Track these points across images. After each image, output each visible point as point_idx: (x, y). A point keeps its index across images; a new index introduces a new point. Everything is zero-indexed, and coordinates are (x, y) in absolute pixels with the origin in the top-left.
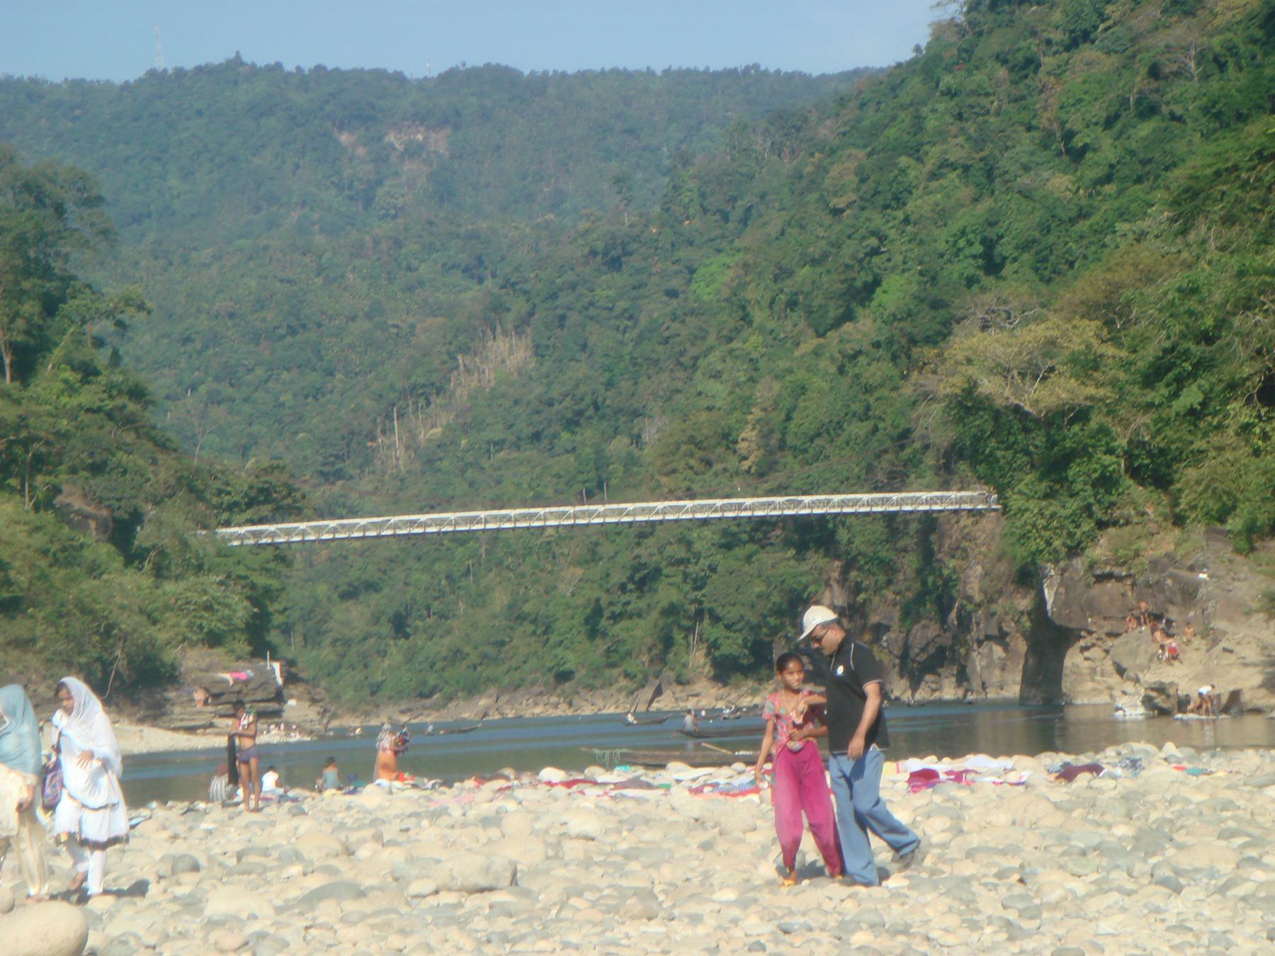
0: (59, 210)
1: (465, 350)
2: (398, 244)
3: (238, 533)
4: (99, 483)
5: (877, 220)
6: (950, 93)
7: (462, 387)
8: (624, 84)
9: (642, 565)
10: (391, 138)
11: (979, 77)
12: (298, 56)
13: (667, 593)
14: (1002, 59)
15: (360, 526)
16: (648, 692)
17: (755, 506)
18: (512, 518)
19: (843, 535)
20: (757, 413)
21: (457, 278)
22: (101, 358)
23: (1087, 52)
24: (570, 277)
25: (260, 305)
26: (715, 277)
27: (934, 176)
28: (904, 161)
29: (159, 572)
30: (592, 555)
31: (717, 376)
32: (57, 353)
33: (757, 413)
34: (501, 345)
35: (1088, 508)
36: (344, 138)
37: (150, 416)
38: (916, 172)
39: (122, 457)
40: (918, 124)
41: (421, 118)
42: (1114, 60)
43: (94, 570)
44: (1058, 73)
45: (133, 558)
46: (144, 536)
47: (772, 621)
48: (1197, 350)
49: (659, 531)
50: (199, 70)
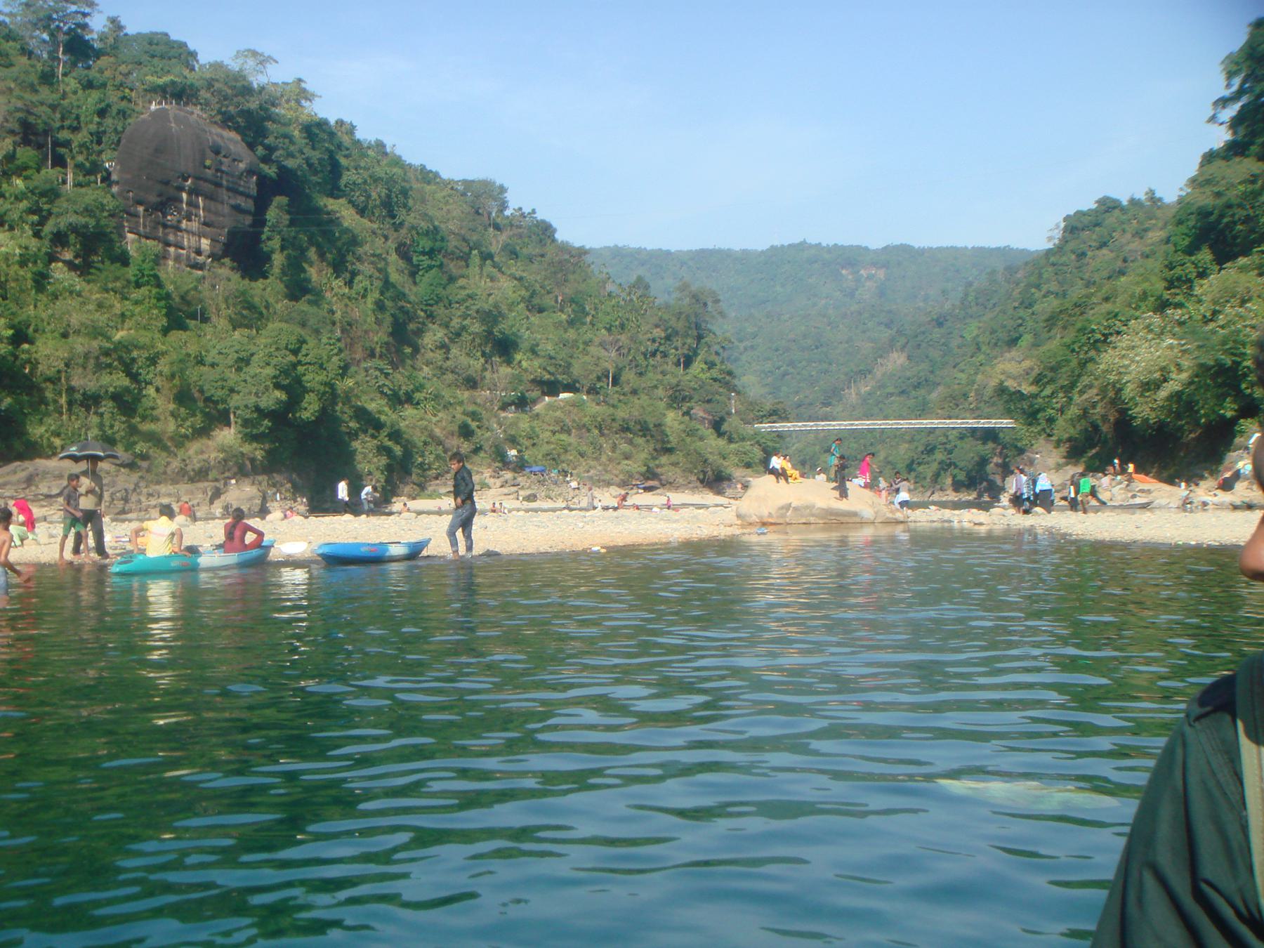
0: (705, 304)
1: (881, 357)
2: (860, 313)
3: (765, 427)
4: (708, 406)
5: (1021, 313)
6: (1053, 265)
7: (879, 372)
8: (955, 253)
9: (929, 445)
10: (862, 272)
11: (1064, 259)
12: (827, 240)
13: (939, 456)
14: (1073, 252)
15: (834, 425)
16: (929, 493)
17: (972, 423)
18: (891, 424)
19: (1001, 435)
20: (976, 386)
21: (882, 328)
22: (717, 360)
23: (1105, 251)
24: (922, 329)
25: (805, 336)
26: (972, 330)
27: (1044, 296)
28: (1033, 290)
29: (731, 440)
30: (912, 441)
31: (962, 371)
32: (699, 358)
33: (976, 386)
34: (895, 355)
35: (1044, 430)
36: (844, 272)
37: (736, 382)
38: (1038, 295)
39: (718, 397)
40: (1040, 275)
41: (874, 264)
42: (1112, 255)
43: (701, 439)
44: (1093, 258)
45: (720, 434)
46: (725, 427)
47: (57, 442)
48: (1050, 375)
49: (937, 432)
50: (790, 245)
